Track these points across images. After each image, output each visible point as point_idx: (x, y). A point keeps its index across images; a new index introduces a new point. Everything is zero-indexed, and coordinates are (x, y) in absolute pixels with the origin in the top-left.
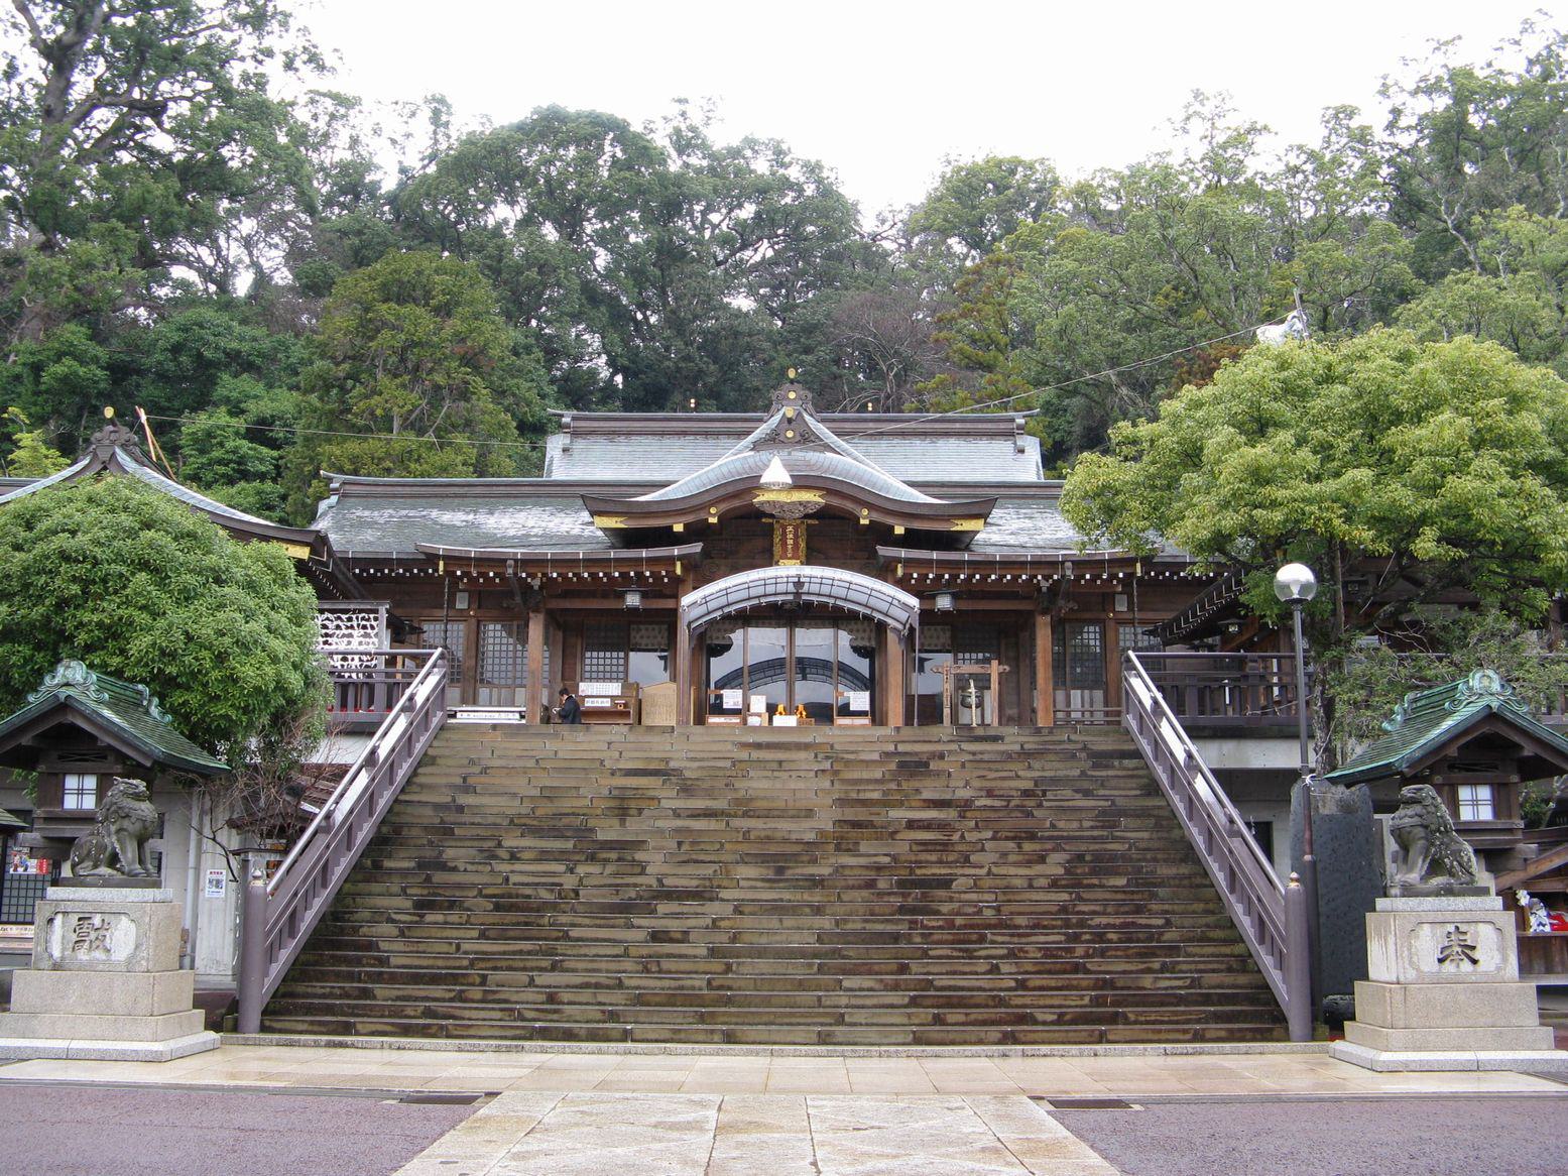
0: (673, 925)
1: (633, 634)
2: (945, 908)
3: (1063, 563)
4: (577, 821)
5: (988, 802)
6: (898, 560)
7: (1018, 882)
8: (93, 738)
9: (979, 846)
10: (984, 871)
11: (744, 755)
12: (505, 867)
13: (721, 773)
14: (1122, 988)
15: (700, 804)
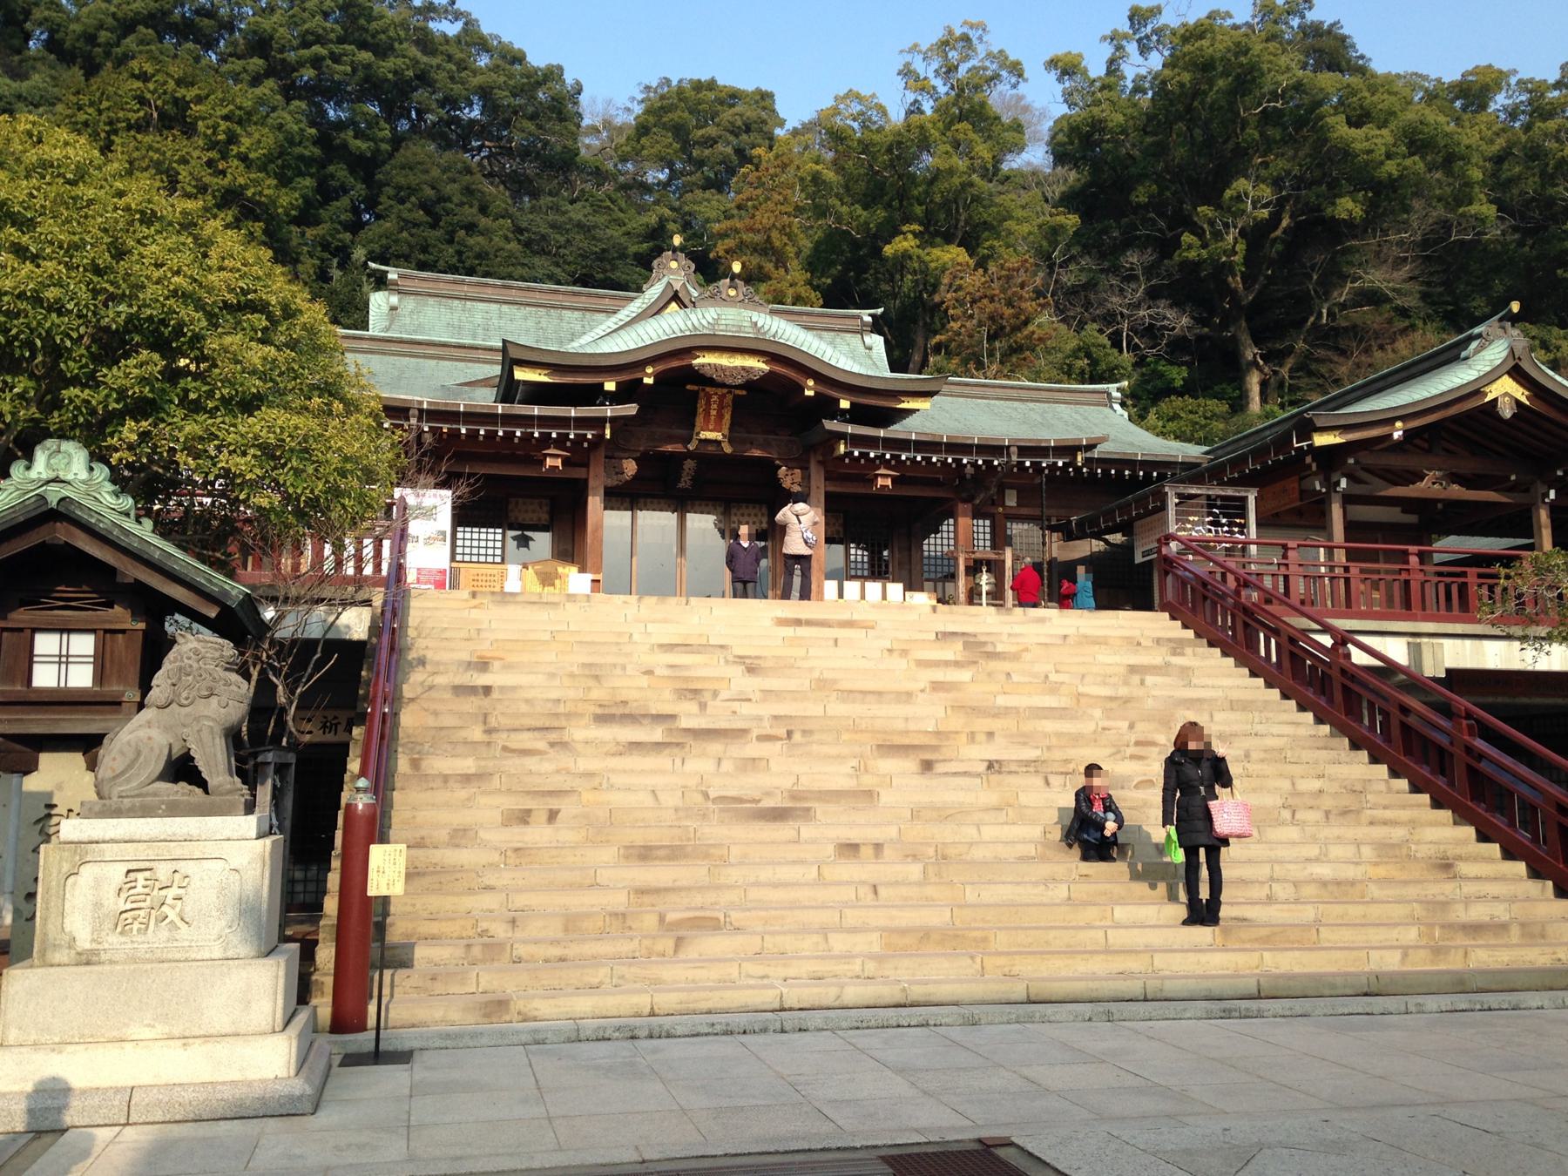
3: (1008, 447)
6: (842, 436)
8: (112, 571)
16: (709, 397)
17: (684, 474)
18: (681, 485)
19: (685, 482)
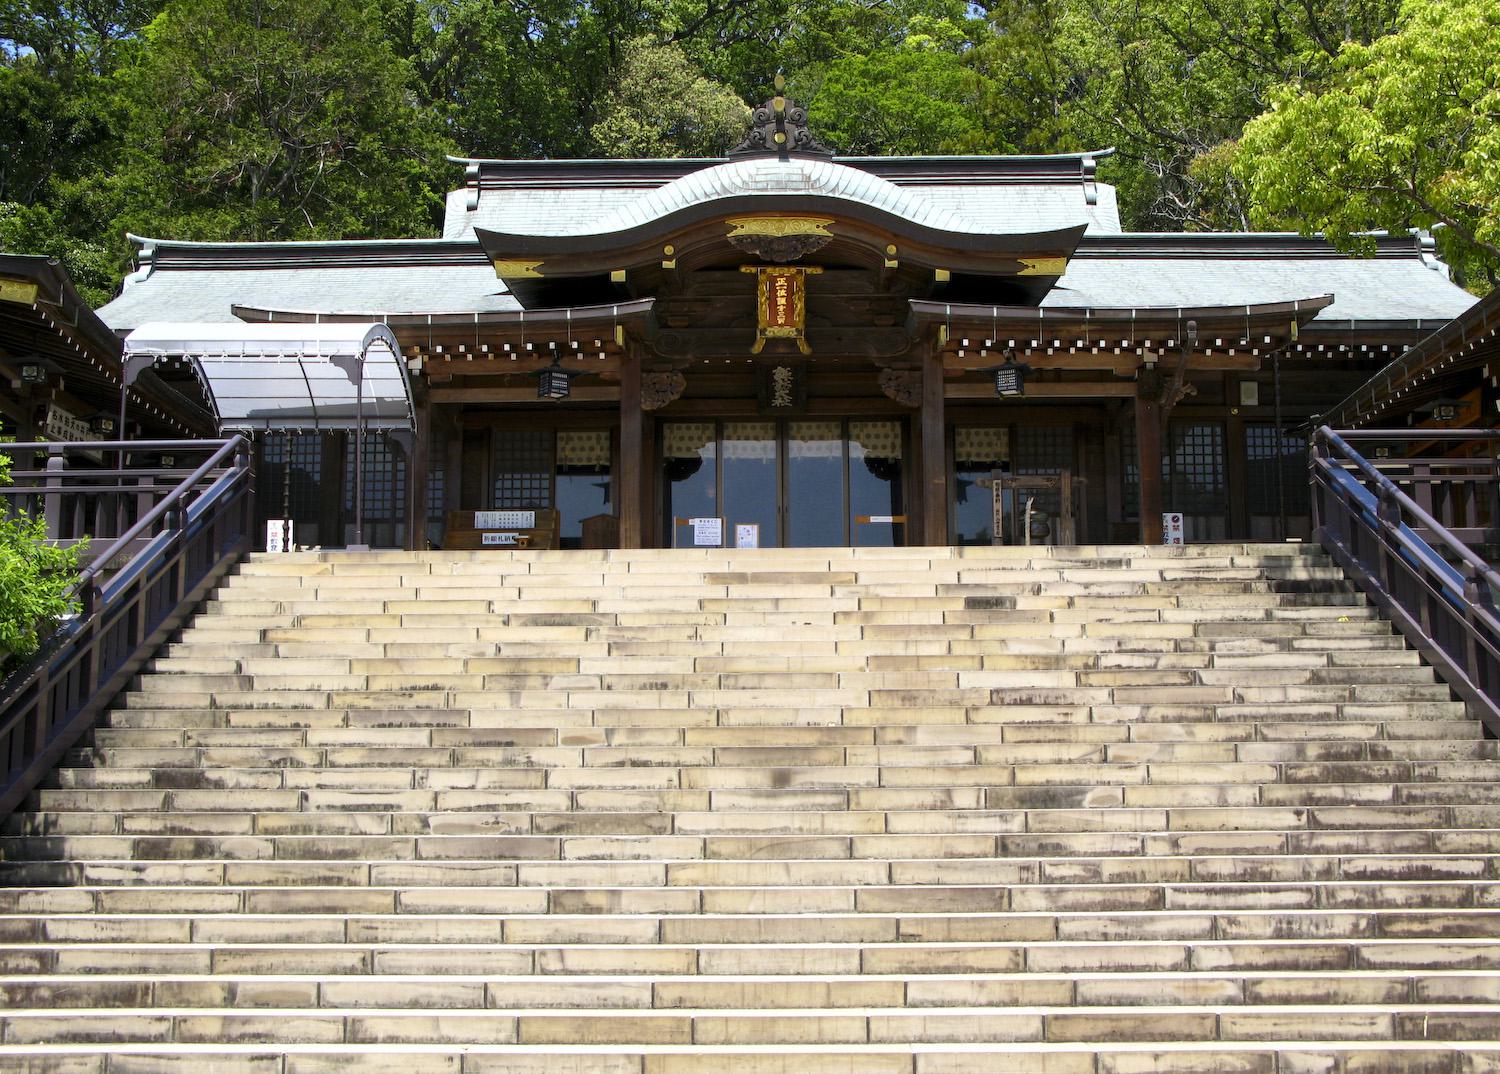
0: (595, 879)
1: (560, 445)
2: (1080, 843)
3: (1184, 320)
4: (436, 700)
5: (1125, 660)
6: (942, 319)
7: (1200, 796)
9: (1122, 732)
10: (1139, 774)
11: (718, 591)
12: (306, 779)
13: (679, 620)
14: (1440, 1000)
15: (644, 667)
16: (773, 280)
17: (778, 387)
18: (778, 402)
19: (781, 398)
